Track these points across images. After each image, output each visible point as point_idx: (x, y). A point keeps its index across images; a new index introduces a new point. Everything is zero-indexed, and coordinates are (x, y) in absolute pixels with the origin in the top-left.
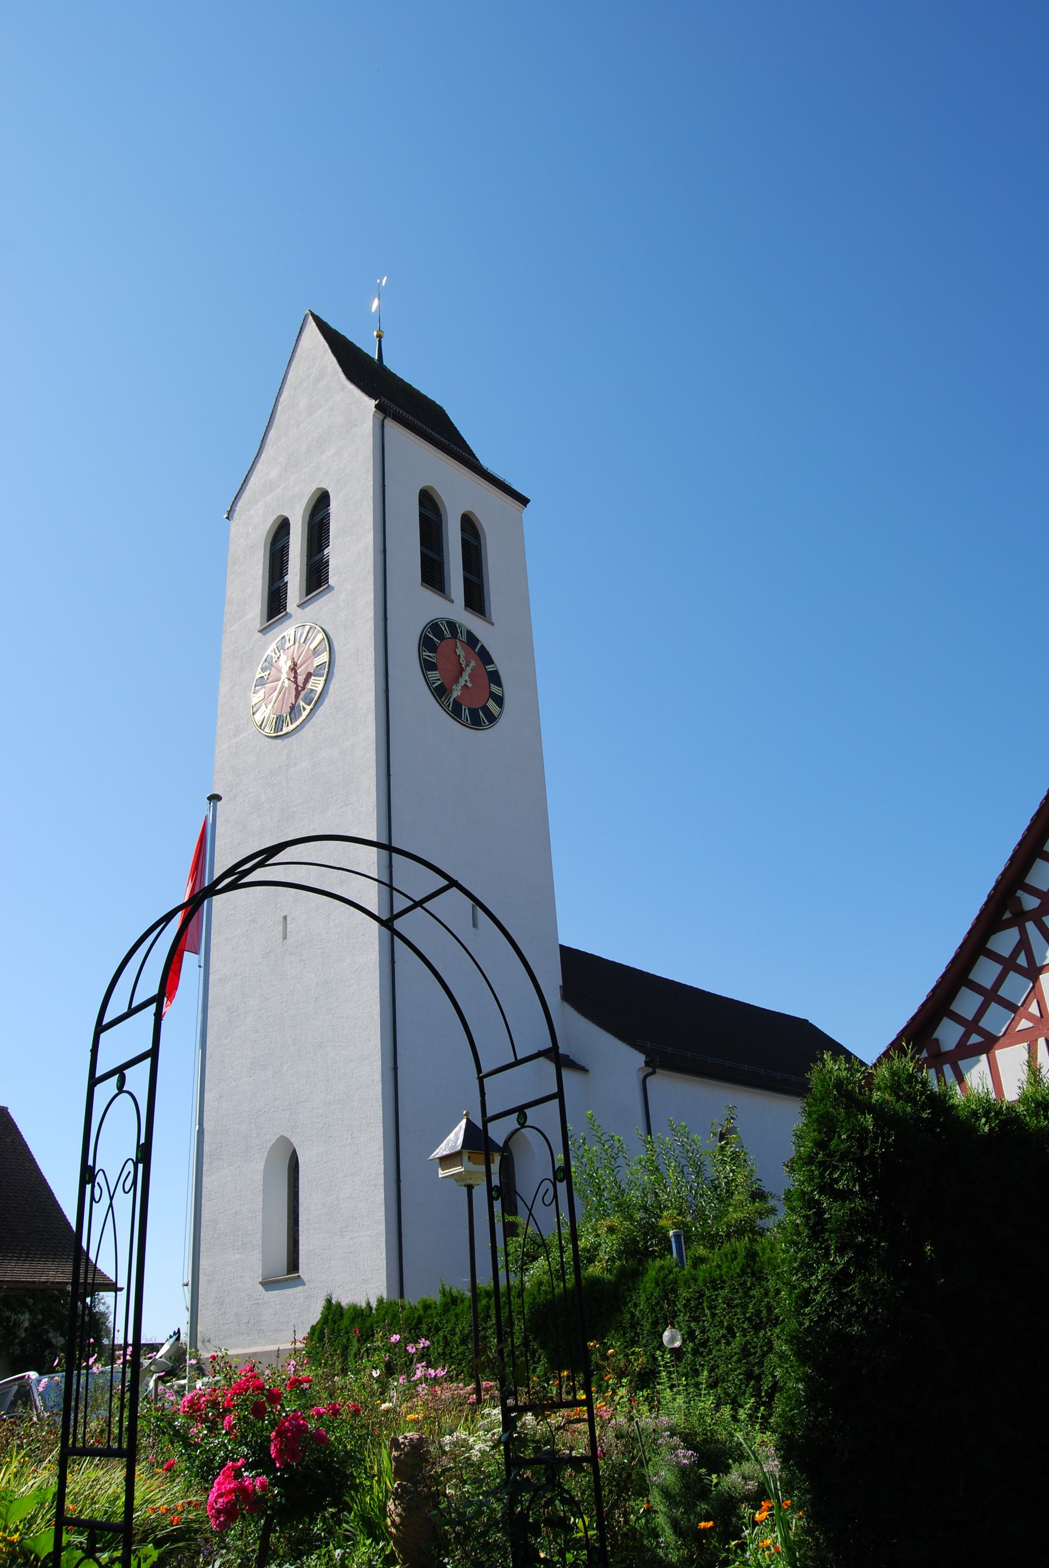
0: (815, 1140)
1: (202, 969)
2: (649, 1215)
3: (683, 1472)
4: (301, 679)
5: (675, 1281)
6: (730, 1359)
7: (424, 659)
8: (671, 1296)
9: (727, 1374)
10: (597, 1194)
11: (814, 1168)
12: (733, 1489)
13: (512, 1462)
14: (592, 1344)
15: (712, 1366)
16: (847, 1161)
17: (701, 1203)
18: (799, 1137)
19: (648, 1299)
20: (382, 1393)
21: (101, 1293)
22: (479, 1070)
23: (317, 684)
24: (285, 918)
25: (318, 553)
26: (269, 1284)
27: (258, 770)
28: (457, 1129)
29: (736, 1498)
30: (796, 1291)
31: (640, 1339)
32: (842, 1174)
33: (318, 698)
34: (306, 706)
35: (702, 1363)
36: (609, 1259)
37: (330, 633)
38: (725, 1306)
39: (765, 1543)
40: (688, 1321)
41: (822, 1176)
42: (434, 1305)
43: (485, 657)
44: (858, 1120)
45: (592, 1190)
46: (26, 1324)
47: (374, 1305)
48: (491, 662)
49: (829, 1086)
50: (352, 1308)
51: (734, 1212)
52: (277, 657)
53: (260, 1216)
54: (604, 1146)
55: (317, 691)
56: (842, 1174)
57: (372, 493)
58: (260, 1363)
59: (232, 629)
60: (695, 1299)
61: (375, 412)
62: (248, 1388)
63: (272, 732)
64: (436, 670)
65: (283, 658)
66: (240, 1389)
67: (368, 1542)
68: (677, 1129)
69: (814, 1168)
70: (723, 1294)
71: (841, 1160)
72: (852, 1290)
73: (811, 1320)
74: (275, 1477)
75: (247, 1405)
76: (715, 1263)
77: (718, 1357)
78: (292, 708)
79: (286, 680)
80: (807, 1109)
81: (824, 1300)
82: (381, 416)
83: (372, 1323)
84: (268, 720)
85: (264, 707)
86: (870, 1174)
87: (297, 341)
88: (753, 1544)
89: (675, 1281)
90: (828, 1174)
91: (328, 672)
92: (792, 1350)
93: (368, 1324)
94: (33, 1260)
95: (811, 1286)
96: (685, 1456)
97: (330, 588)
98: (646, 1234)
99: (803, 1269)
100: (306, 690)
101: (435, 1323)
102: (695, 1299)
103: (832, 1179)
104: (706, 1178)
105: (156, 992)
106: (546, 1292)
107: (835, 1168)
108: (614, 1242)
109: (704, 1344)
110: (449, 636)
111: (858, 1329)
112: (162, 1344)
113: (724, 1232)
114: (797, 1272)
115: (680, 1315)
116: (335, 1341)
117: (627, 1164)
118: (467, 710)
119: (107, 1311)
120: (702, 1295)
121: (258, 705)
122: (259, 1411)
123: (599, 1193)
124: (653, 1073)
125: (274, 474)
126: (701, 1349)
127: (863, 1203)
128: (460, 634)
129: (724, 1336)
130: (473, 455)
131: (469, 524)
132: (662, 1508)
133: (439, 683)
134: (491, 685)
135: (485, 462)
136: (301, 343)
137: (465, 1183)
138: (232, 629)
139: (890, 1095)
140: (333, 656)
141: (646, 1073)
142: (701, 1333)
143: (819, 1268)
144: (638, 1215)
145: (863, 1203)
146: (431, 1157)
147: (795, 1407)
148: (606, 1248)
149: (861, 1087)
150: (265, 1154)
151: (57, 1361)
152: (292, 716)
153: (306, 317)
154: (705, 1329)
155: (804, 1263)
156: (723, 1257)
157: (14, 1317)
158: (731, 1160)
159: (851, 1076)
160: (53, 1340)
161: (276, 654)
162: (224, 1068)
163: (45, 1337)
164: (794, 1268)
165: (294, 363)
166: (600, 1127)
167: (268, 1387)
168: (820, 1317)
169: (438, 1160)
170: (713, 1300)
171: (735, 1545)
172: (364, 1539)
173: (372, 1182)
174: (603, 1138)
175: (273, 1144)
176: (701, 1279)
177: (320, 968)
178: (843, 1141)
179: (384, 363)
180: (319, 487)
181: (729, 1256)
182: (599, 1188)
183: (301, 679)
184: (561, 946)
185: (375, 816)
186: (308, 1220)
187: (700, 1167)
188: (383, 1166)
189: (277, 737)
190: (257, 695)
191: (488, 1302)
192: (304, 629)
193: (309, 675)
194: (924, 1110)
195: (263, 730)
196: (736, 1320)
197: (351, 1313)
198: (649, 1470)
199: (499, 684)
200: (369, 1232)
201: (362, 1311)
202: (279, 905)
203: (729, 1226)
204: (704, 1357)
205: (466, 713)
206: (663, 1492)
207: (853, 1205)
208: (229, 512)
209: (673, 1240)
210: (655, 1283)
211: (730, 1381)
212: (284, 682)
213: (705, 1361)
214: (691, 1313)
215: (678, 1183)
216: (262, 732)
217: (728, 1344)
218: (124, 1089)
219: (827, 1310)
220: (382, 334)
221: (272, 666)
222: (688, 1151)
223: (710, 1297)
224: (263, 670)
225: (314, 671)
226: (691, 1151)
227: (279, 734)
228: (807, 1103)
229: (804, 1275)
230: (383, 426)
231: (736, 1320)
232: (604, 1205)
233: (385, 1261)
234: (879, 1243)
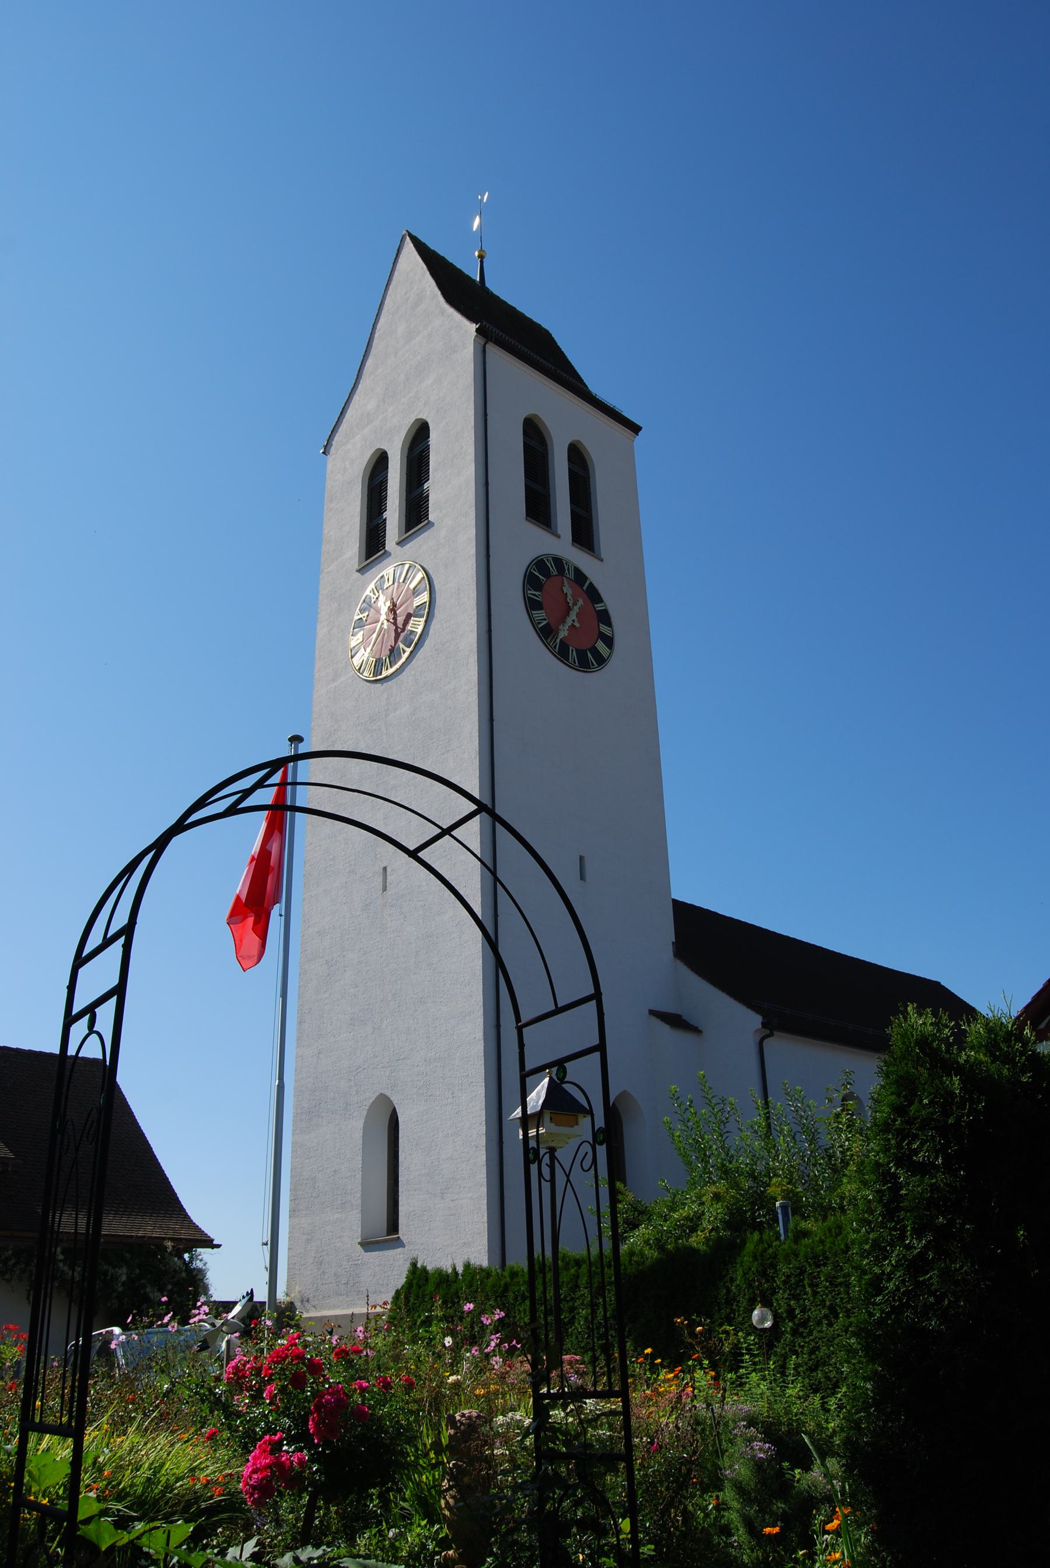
0: (893, 1105)
1: (283, 918)
2: (758, 1183)
3: (758, 1466)
4: (400, 620)
5: (775, 1256)
6: (831, 1342)
7: (529, 598)
8: (770, 1272)
9: (828, 1357)
10: (702, 1160)
11: (890, 1136)
12: (813, 1488)
13: (542, 1454)
14: (679, 1320)
15: (813, 1348)
16: (929, 1129)
17: (814, 1172)
18: (876, 1101)
19: (745, 1274)
20: (452, 1365)
21: (199, 1250)
22: (518, 1018)
23: (417, 626)
24: (385, 869)
25: (418, 487)
26: (368, 1245)
27: (356, 716)
28: (539, 1087)
29: (816, 1498)
30: (867, 1277)
31: (736, 1317)
32: (922, 1144)
33: (419, 640)
35: (802, 1344)
36: (713, 1229)
37: (431, 572)
38: (828, 1284)
39: (833, 1557)
40: (787, 1299)
41: (899, 1146)
42: (521, 1273)
43: (594, 595)
44: (943, 1083)
45: (698, 1155)
46: (124, 1278)
47: (460, 1269)
48: (600, 600)
49: (910, 1043)
50: (437, 1273)
51: (848, 1183)
52: (375, 597)
53: (359, 1175)
54: (713, 1109)
55: (417, 633)
56: (922, 1144)
57: (473, 423)
58: (339, 1326)
59: (329, 569)
60: (796, 1276)
61: (476, 336)
62: (287, 1356)
63: (371, 676)
65: (382, 598)
66: (278, 1356)
67: (423, 1523)
68: (792, 1093)
69: (890, 1136)
70: (826, 1272)
71: (922, 1128)
72: (931, 1278)
73: (882, 1311)
74: (317, 1453)
75: (285, 1374)
76: (818, 1238)
77: (820, 1339)
78: (392, 650)
79: (385, 622)
80: (884, 1068)
81: (898, 1289)
82: (482, 341)
83: (457, 1290)
84: (367, 663)
85: (362, 649)
86: (955, 1145)
88: (823, 1555)
89: (775, 1256)
90: (907, 1144)
91: (428, 613)
92: (859, 1343)
93: (453, 1290)
94: (144, 1216)
95: (883, 1272)
96: (762, 1449)
97: (430, 524)
98: (753, 1204)
99: (875, 1252)
100: (406, 632)
101: (521, 1292)
102: (796, 1276)
103: (910, 1150)
104: (820, 1147)
105: (126, 922)
106: (637, 1263)
107: (915, 1137)
108: (719, 1211)
109: (804, 1324)
110: (555, 573)
111: (936, 1323)
112: (235, 1303)
113: (837, 1204)
114: (869, 1254)
115: (779, 1292)
116: (419, 1307)
117: (739, 1129)
118: (574, 653)
119: (204, 1268)
120: (803, 1271)
121: (356, 648)
122: (298, 1381)
123: (705, 1160)
124: (771, 1035)
125: (371, 406)
126: (801, 1330)
127: (946, 1178)
128: (567, 571)
129: (826, 1316)
130: (584, 384)
131: (577, 455)
132: (735, 1504)
133: (545, 623)
134: (601, 625)
135: (594, 388)
136: (399, 266)
137: (547, 1145)
138: (329, 569)
139: (985, 1055)
140: (433, 596)
141: (762, 1035)
142: (801, 1312)
143: (892, 1252)
144: (746, 1184)
145: (946, 1178)
146: (511, 1117)
147: (862, 1409)
148: (710, 1217)
149: (949, 1046)
150: (365, 1113)
151: (130, 1318)
152: (392, 659)
153: (403, 238)
154: (806, 1308)
155: (876, 1245)
156: (827, 1232)
157: (111, 1270)
158: (847, 1128)
159: (937, 1032)
160: (151, 1295)
161: (374, 594)
162: (324, 1023)
163: (142, 1292)
164: (865, 1250)
165: (391, 287)
166: (711, 1088)
167: (309, 1356)
168: (893, 1307)
169: (518, 1121)
170: (815, 1277)
171: (802, 1555)
172: (419, 1520)
173: (473, 1143)
174: (714, 1101)
175: (373, 1102)
176: (802, 1254)
177: (421, 921)
178: (924, 1106)
179: (487, 285)
180: (419, 417)
181: (834, 1230)
182: (705, 1154)
183: (400, 620)
184: (675, 902)
185: (478, 763)
186: (408, 1181)
187: (814, 1135)
188: (485, 1127)
189: (376, 681)
190: (355, 638)
191: (576, 1271)
192: (403, 568)
193: (409, 616)
194: (1024, 1073)
195: (362, 674)
196: (839, 1300)
197: (436, 1278)
198: (726, 1462)
199: (609, 624)
200: (471, 1194)
201: (448, 1276)
202: (379, 856)
203: (842, 1198)
204: (804, 1338)
205: (573, 655)
206: (736, 1487)
207: (934, 1181)
208: (326, 447)
209: (779, 1211)
210: (753, 1257)
211: (831, 1365)
212: (382, 624)
213: (806, 1343)
214: (791, 1291)
215: (790, 1151)
216: (361, 676)
217: (830, 1325)
218: (94, 1029)
219: (900, 1300)
220: (483, 254)
221: (371, 606)
222: (802, 1117)
223: (811, 1274)
224: (362, 611)
225: (414, 612)
226: (805, 1117)
227: (378, 678)
228: (885, 1062)
229: (877, 1258)
230: (484, 351)
231: (839, 1300)
232: (710, 1173)
233: (486, 1225)
234: (963, 1225)
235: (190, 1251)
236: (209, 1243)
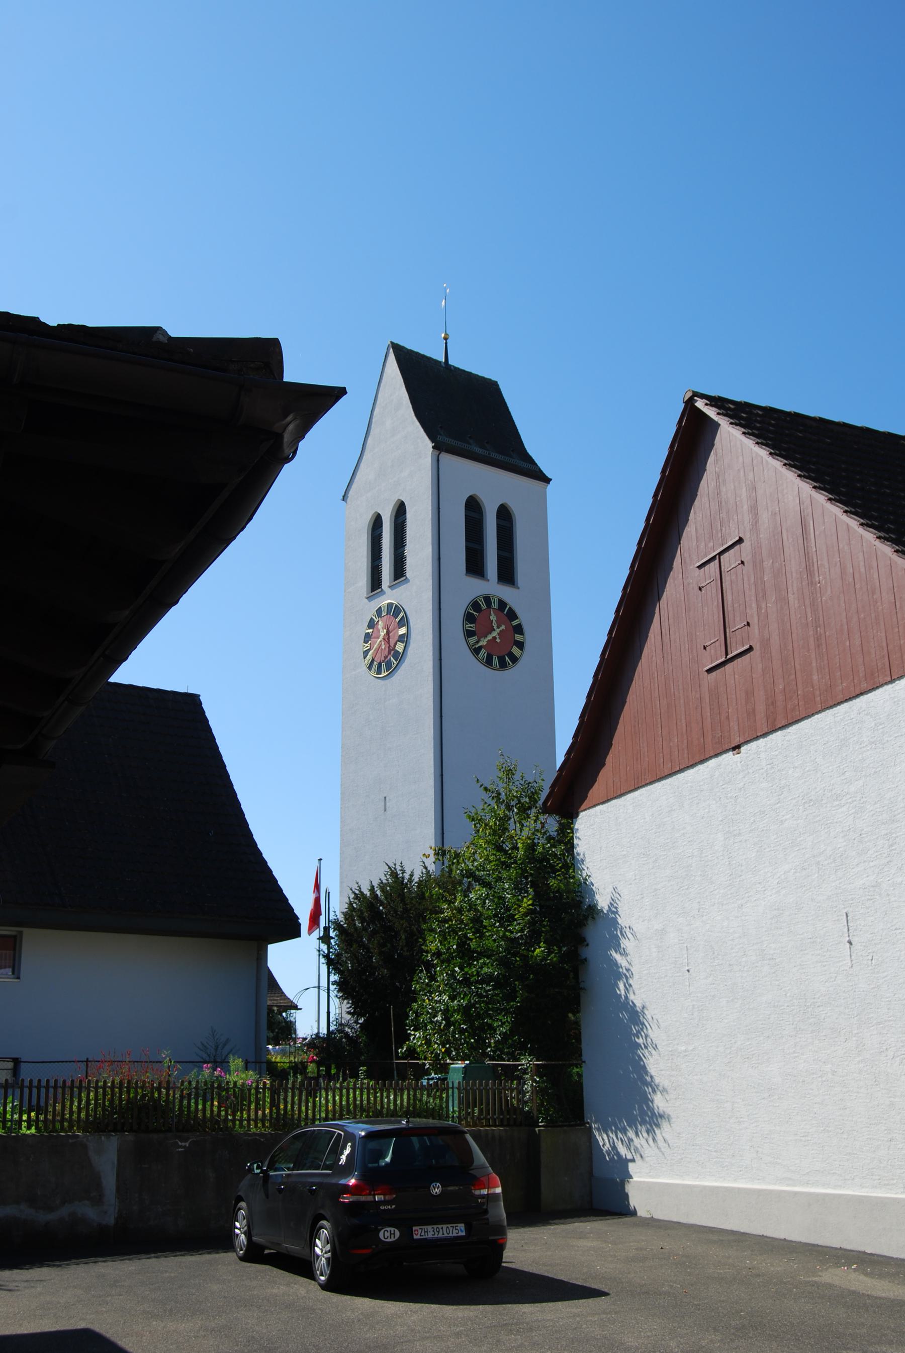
7: (467, 630)
24: (385, 798)
34: (395, 662)
43: (512, 615)
64: (475, 636)
87: (383, 366)
91: (407, 641)
97: (407, 580)
118: (497, 659)
128: (493, 604)
165: (382, 384)
220: (447, 337)
235: (286, 1012)
236: (296, 1007)
